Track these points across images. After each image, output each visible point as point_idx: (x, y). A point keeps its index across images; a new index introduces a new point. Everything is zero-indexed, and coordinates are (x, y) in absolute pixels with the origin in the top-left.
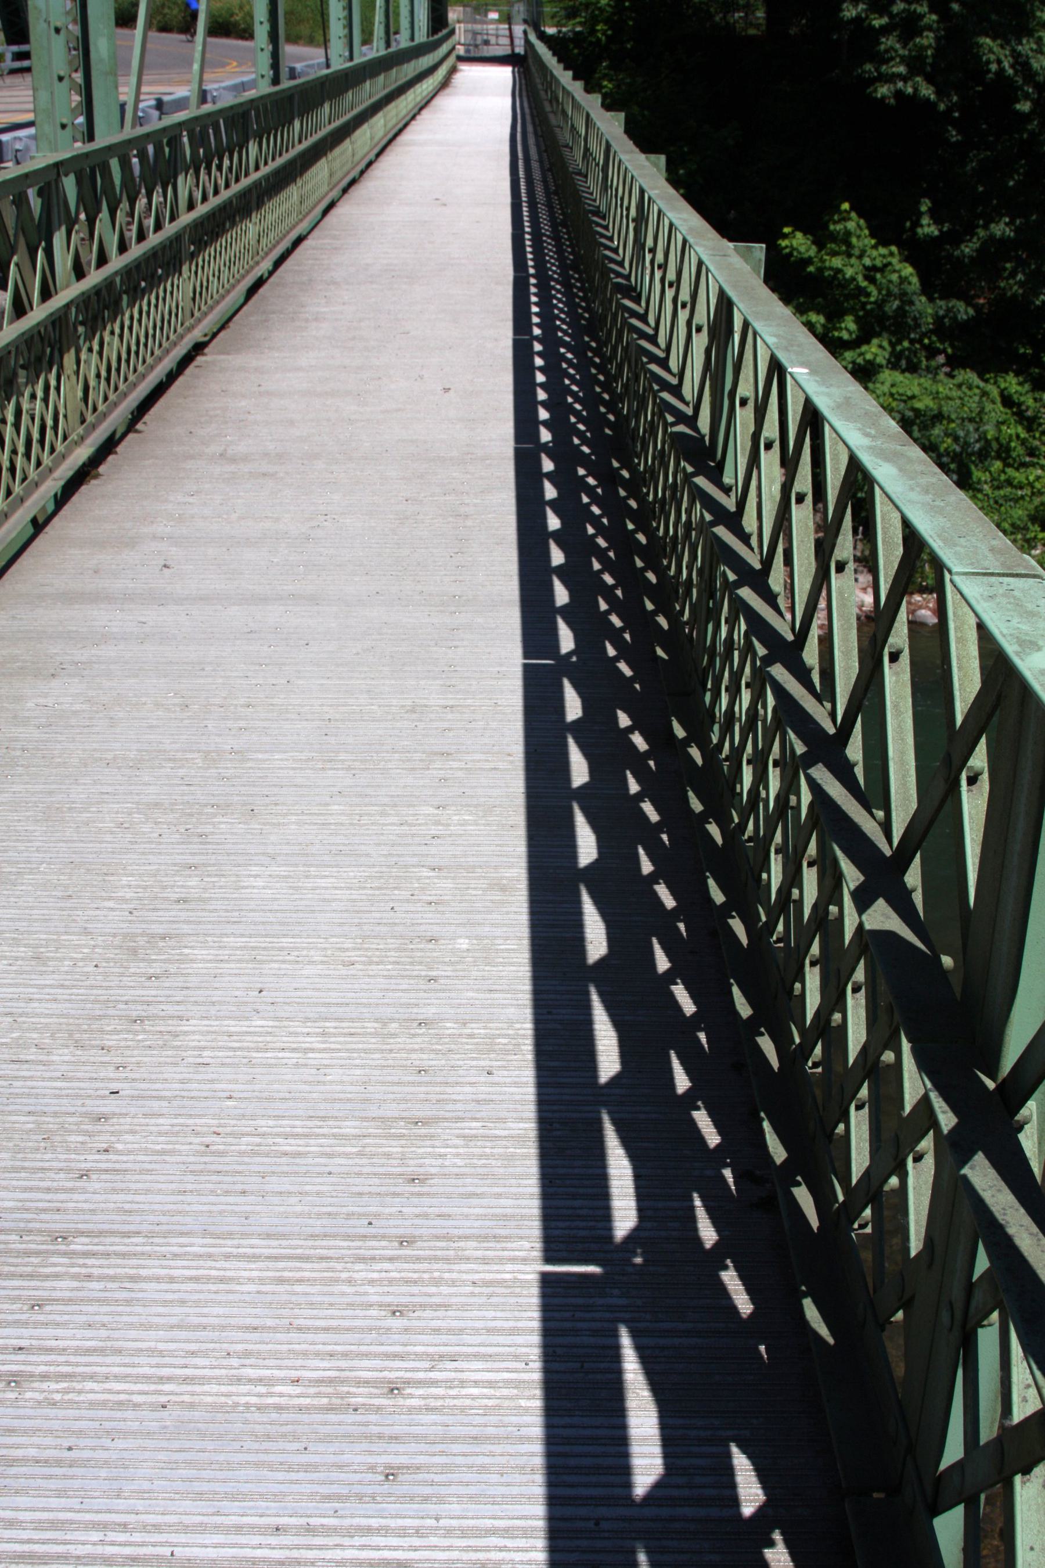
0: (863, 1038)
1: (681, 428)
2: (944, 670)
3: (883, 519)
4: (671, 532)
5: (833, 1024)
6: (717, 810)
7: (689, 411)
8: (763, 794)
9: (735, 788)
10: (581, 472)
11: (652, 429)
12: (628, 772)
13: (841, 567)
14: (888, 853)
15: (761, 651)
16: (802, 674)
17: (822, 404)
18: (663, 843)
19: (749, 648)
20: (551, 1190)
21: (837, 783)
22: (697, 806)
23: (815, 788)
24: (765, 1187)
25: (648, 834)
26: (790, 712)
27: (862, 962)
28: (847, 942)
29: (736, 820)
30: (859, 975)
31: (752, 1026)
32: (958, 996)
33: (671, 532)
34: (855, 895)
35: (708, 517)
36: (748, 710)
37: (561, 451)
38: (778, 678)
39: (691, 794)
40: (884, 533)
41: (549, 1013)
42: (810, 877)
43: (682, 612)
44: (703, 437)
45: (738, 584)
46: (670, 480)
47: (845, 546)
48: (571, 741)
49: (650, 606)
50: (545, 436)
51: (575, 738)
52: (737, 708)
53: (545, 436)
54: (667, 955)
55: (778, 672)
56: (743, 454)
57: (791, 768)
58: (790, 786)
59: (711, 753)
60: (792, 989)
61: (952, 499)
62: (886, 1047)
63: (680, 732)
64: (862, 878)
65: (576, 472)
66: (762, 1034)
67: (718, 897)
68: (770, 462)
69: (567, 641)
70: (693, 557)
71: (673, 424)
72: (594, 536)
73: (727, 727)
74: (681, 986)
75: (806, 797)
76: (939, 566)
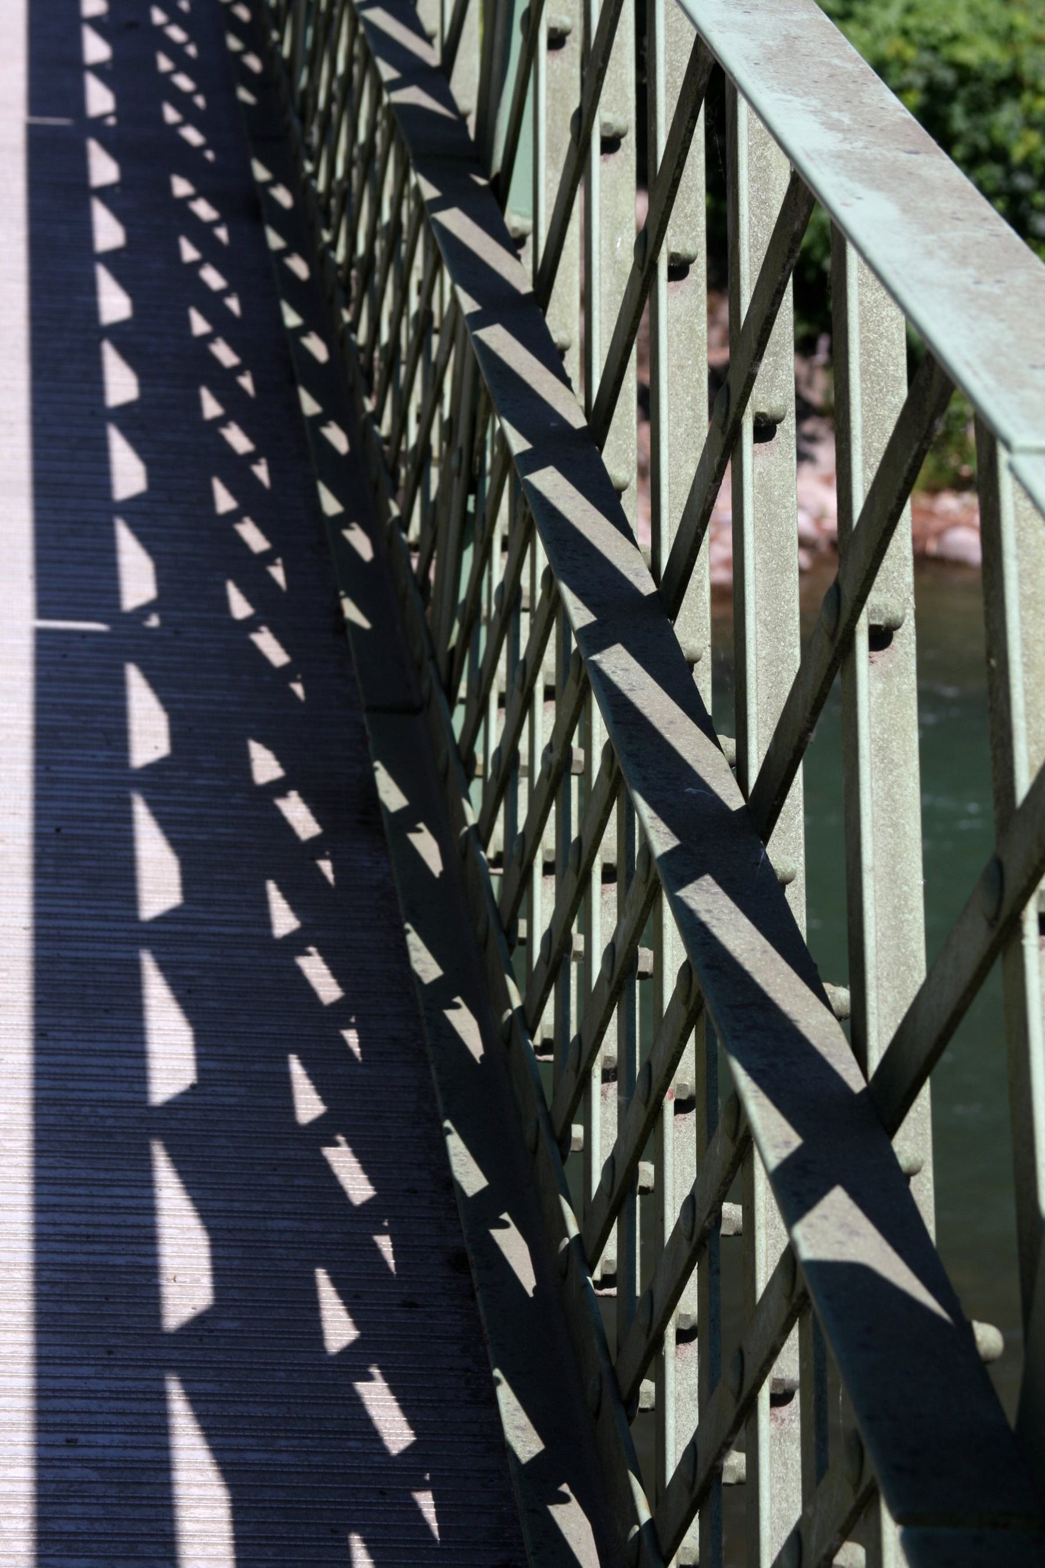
0: (795, 1513)
1: (413, 95)
2: (991, 671)
3: (864, 321)
4: (385, 336)
5: (728, 1478)
6: (473, 975)
7: (433, 56)
8: (578, 943)
9: (515, 927)
10: (181, 187)
11: (346, 95)
12: (271, 887)
13: (765, 430)
14: (857, 1083)
15: (581, 615)
16: (672, 671)
17: (735, 54)
18: (323, 877)
19: (553, 609)
20: (44, 1044)
21: (746, 921)
22: (426, 966)
23: (695, 931)
24: (450, 1237)
25: (291, 862)
26: (640, 750)
27: (795, 1334)
28: (761, 1287)
29: (516, 1002)
30: (788, 1364)
31: (541, 1480)
32: (1012, 1419)
33: (385, 336)
34: (779, 1178)
35: (469, 305)
36: (549, 748)
37: (140, 142)
38: (618, 678)
39: (413, 939)
40: (866, 353)
41: (71, 1443)
42: (680, 1135)
43: (404, 522)
44: (463, 117)
45: (533, 461)
46: (386, 215)
47: (777, 379)
48: (141, 811)
49: (331, 505)
50: (99, 100)
51: (150, 803)
52: (523, 746)
53: (99, 100)
54: (351, 1312)
55: (618, 664)
56: (552, 161)
57: (646, 886)
58: (639, 926)
59: (462, 847)
60: (635, 1393)
61: (1021, 278)
62: (846, 1534)
63: (392, 796)
64: (796, 1141)
65: (168, 187)
66: (564, 1499)
67: (470, 1177)
68: (613, 178)
69: (137, 579)
70: (434, 395)
71: (395, 85)
72: (208, 338)
73: (501, 789)
74: (345, 1149)
75: (675, 953)
76: (990, 439)
